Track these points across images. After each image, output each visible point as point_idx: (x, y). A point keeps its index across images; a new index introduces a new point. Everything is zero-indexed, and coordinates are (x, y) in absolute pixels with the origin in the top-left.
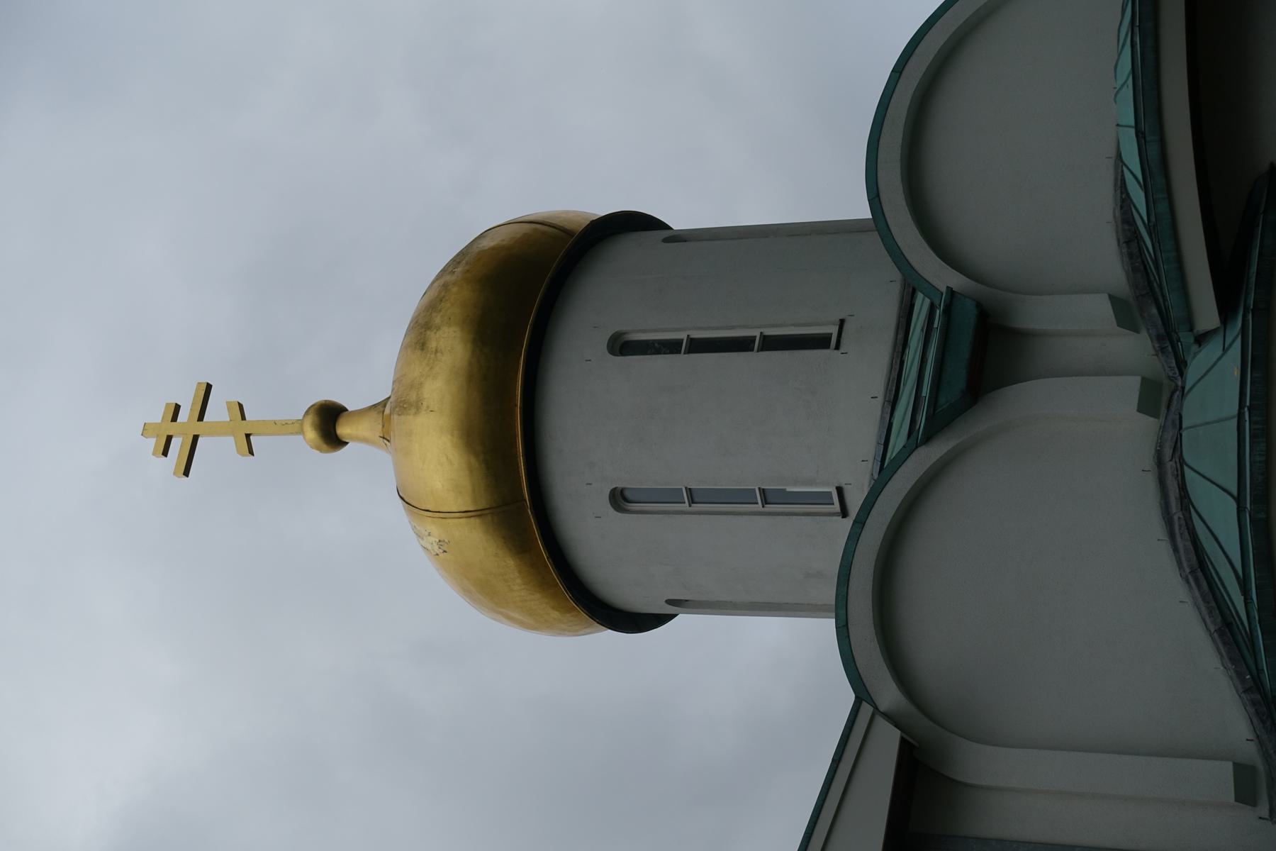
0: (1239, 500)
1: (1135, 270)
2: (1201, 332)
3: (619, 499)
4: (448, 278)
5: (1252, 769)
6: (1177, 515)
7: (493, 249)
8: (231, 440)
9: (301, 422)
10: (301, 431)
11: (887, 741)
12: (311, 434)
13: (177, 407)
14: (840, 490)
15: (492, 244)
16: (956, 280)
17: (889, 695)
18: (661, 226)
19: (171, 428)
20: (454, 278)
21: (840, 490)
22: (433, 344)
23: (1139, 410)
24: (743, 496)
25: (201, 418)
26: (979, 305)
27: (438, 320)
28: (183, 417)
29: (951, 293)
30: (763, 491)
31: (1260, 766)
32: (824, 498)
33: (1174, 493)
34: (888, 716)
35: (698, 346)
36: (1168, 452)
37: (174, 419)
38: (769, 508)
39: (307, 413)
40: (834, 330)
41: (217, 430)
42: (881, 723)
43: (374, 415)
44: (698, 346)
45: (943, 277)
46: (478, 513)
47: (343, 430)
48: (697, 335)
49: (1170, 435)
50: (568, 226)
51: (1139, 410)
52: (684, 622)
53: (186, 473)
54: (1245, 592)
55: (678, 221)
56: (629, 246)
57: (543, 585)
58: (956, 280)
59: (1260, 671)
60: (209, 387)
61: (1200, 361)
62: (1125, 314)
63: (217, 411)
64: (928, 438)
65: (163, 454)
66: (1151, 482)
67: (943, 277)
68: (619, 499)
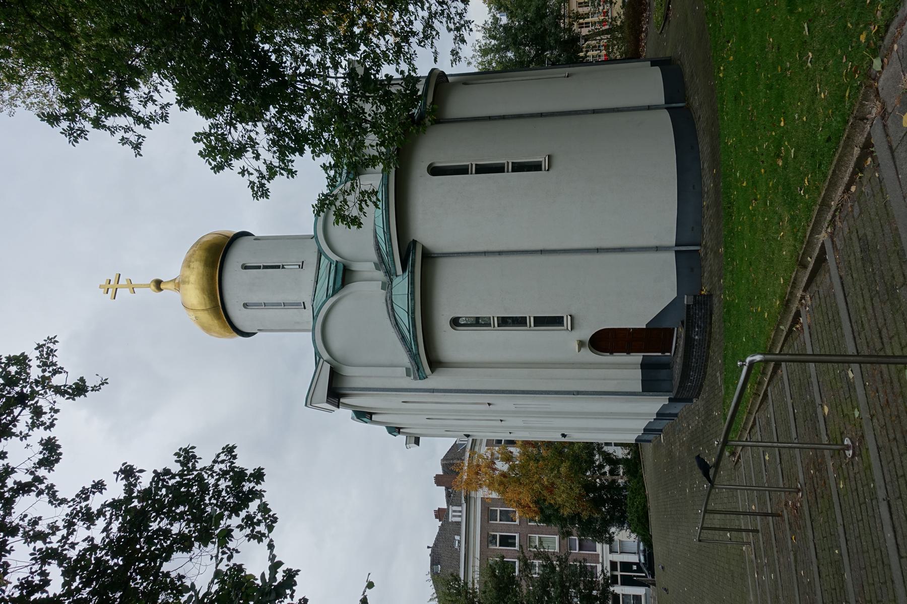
0: (408, 313)
1: (379, 256)
2: (379, 260)
3: (246, 305)
4: (194, 248)
5: (410, 369)
6: (391, 313)
7: (208, 241)
8: (128, 289)
9: (150, 284)
10: (150, 287)
11: (327, 368)
12: (153, 287)
13: (110, 280)
14: (304, 303)
15: (208, 239)
16: (338, 259)
17: (326, 356)
18: (252, 235)
19: (109, 286)
20: (196, 249)
21: (304, 303)
22: (192, 266)
23: (382, 289)
24: (279, 304)
25: (118, 283)
26: (343, 265)
27: (193, 260)
28: (112, 283)
29: (337, 262)
30: (284, 303)
31: (411, 367)
32: (298, 304)
33: (390, 308)
34: (326, 361)
35: (266, 267)
36: (388, 299)
37: (109, 283)
38: (286, 307)
39: (151, 282)
40: (301, 264)
41: (123, 287)
42: (325, 362)
43: (172, 283)
44: (266, 267)
45: (335, 258)
46: (207, 310)
47: (162, 286)
48: (265, 264)
49: (389, 295)
50: (227, 235)
51: (382, 289)
52: (259, 334)
53: (114, 298)
54: (409, 332)
55: (257, 234)
56: (244, 241)
57: (225, 327)
58: (338, 259)
59: (412, 349)
60: (120, 275)
61: (396, 281)
62: (377, 268)
63: (123, 281)
64: (332, 296)
65: (415, 443)
66: (385, 305)
67: (335, 258)
68: (246, 305)
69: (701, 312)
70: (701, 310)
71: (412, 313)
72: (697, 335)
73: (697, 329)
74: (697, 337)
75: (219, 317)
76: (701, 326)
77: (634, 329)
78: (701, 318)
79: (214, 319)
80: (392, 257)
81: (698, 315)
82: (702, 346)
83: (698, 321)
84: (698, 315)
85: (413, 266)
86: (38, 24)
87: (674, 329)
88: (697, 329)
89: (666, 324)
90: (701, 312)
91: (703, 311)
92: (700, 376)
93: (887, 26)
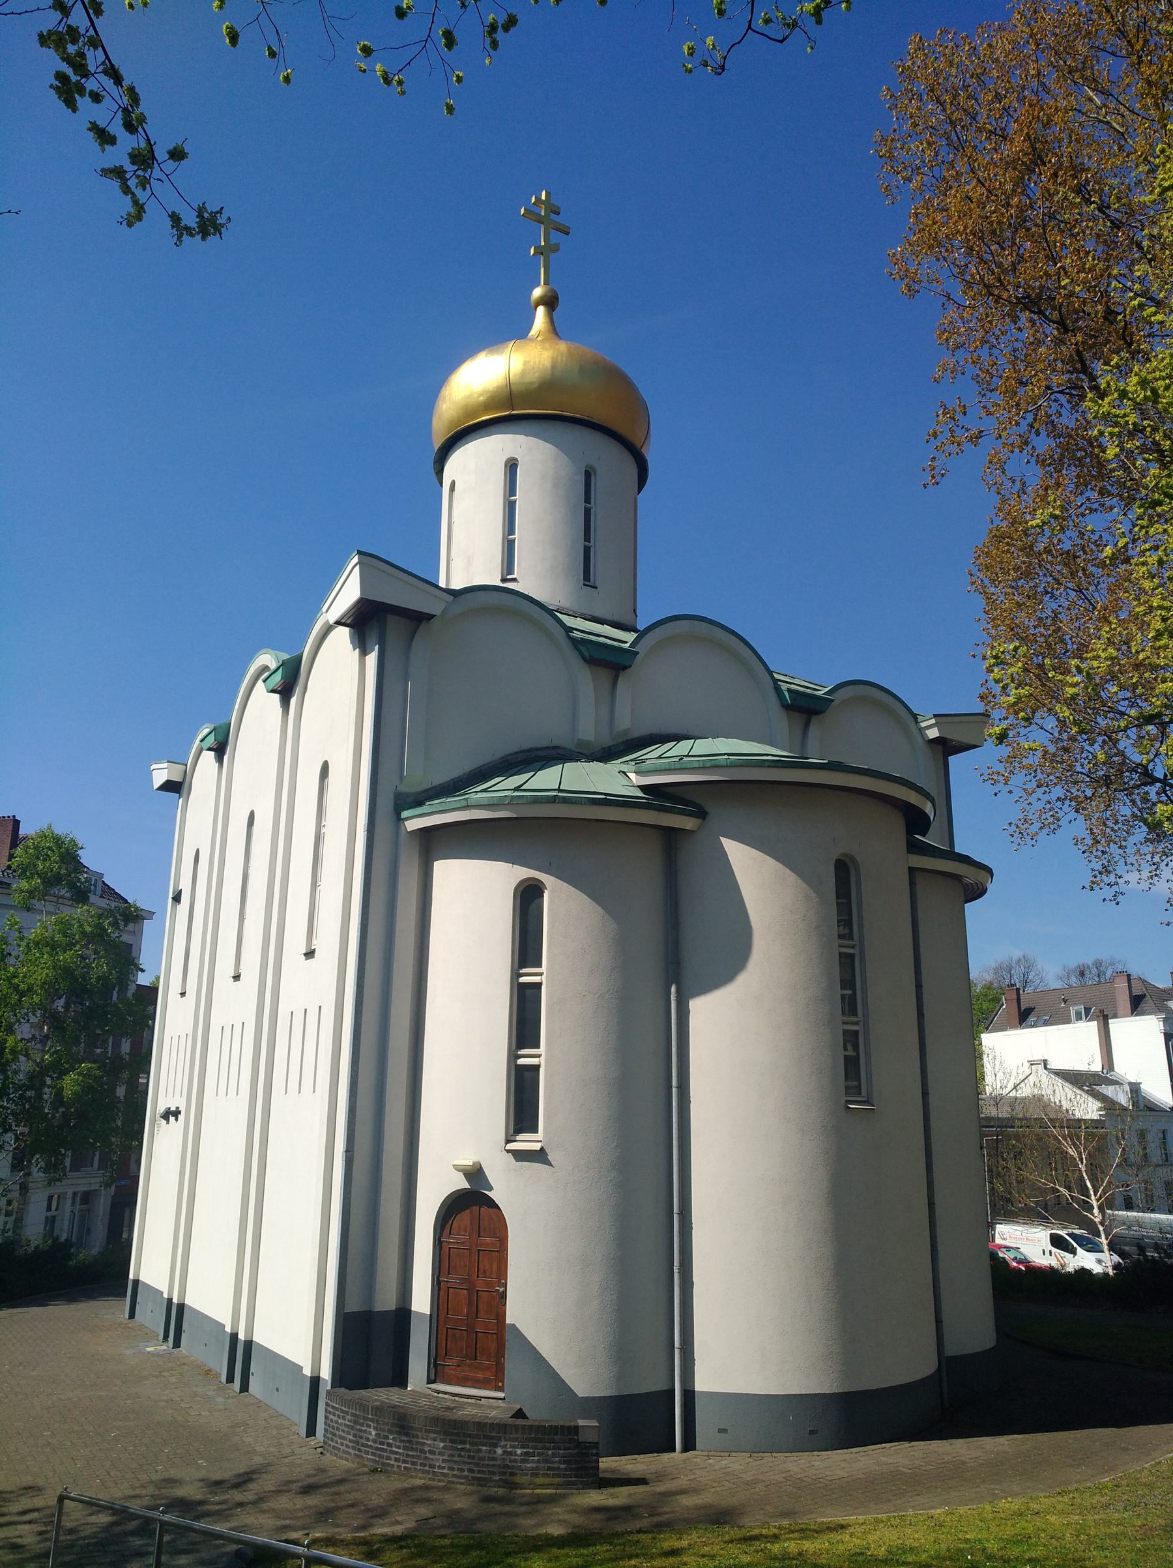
48: (592, 511)
69: (560, 1462)
70: (565, 1462)
71: (564, 798)
72: (505, 1452)
73: (519, 1451)
74: (499, 1451)
75: (488, 406)
76: (527, 1461)
77: (503, 1296)
78: (546, 1461)
79: (488, 395)
80: (678, 766)
81: (554, 1455)
82: (477, 1465)
83: (539, 1455)
84: (554, 1455)
85: (660, 809)
86: (1014, 191)
87: (501, 1389)
88: (519, 1451)
89: (514, 1367)
90: (560, 1462)
91: (562, 1466)
92: (396, 1460)
93: (396, 1562)
